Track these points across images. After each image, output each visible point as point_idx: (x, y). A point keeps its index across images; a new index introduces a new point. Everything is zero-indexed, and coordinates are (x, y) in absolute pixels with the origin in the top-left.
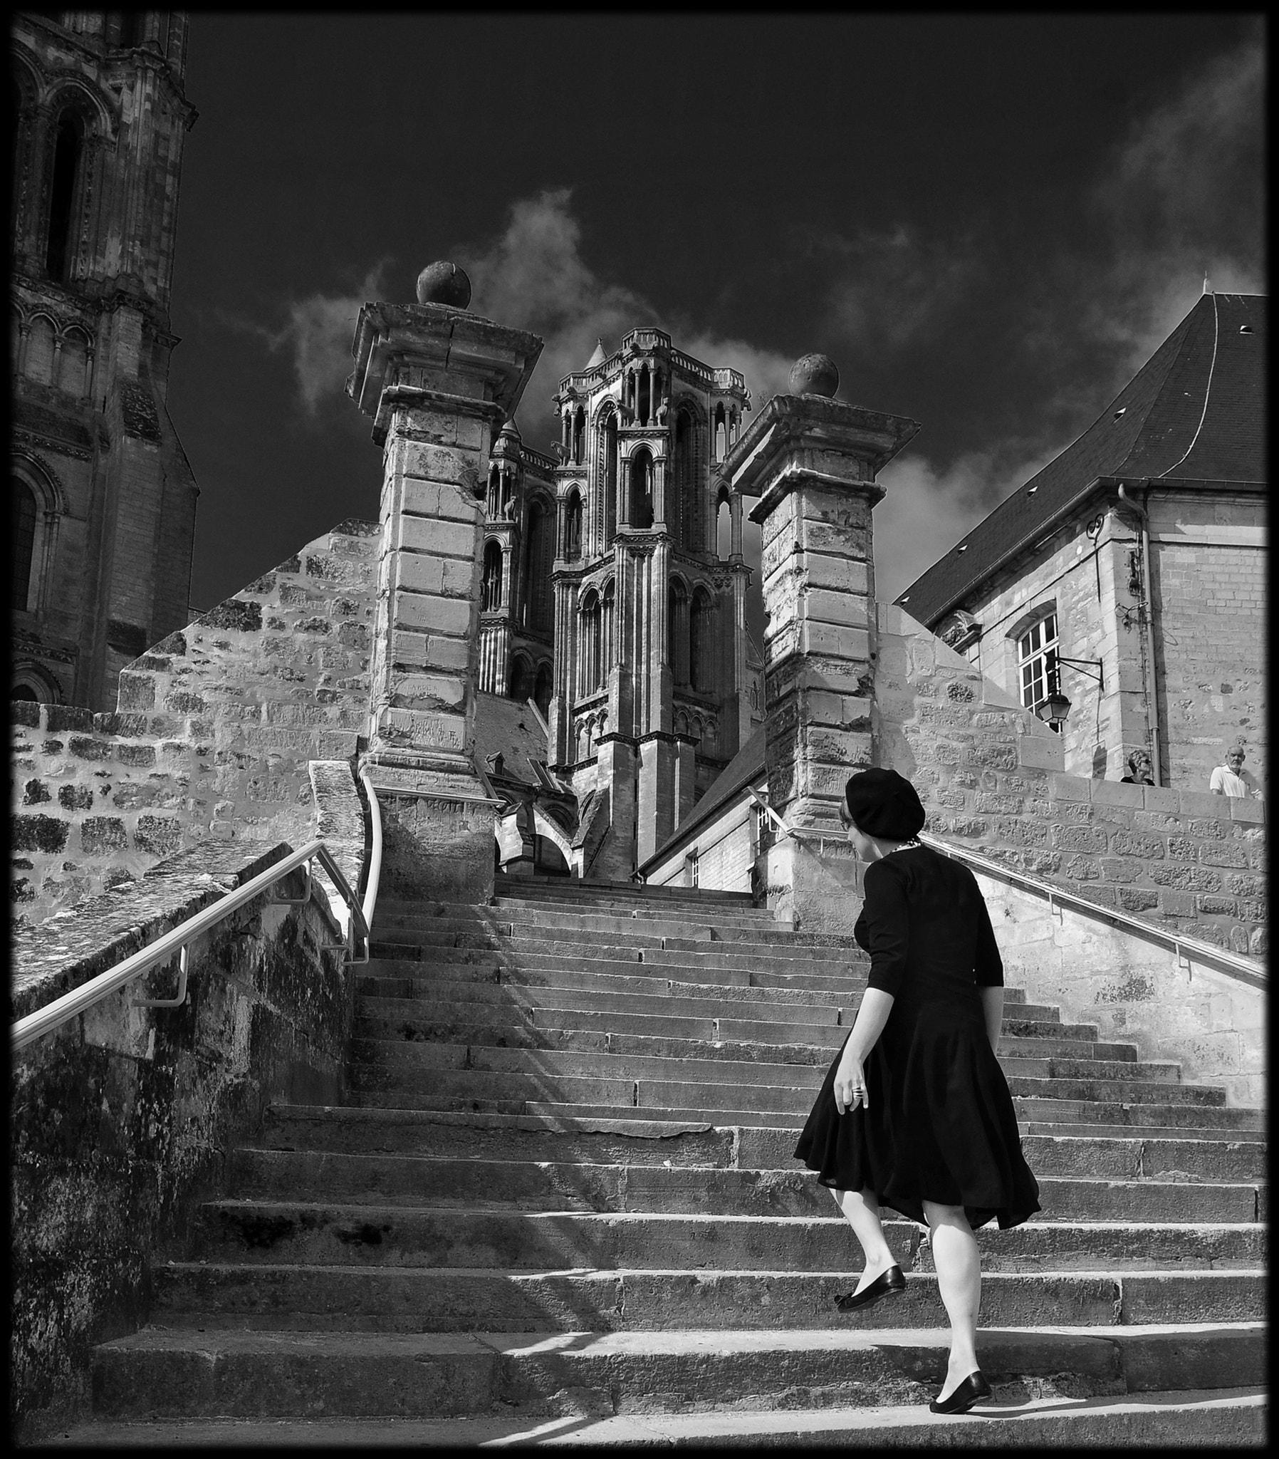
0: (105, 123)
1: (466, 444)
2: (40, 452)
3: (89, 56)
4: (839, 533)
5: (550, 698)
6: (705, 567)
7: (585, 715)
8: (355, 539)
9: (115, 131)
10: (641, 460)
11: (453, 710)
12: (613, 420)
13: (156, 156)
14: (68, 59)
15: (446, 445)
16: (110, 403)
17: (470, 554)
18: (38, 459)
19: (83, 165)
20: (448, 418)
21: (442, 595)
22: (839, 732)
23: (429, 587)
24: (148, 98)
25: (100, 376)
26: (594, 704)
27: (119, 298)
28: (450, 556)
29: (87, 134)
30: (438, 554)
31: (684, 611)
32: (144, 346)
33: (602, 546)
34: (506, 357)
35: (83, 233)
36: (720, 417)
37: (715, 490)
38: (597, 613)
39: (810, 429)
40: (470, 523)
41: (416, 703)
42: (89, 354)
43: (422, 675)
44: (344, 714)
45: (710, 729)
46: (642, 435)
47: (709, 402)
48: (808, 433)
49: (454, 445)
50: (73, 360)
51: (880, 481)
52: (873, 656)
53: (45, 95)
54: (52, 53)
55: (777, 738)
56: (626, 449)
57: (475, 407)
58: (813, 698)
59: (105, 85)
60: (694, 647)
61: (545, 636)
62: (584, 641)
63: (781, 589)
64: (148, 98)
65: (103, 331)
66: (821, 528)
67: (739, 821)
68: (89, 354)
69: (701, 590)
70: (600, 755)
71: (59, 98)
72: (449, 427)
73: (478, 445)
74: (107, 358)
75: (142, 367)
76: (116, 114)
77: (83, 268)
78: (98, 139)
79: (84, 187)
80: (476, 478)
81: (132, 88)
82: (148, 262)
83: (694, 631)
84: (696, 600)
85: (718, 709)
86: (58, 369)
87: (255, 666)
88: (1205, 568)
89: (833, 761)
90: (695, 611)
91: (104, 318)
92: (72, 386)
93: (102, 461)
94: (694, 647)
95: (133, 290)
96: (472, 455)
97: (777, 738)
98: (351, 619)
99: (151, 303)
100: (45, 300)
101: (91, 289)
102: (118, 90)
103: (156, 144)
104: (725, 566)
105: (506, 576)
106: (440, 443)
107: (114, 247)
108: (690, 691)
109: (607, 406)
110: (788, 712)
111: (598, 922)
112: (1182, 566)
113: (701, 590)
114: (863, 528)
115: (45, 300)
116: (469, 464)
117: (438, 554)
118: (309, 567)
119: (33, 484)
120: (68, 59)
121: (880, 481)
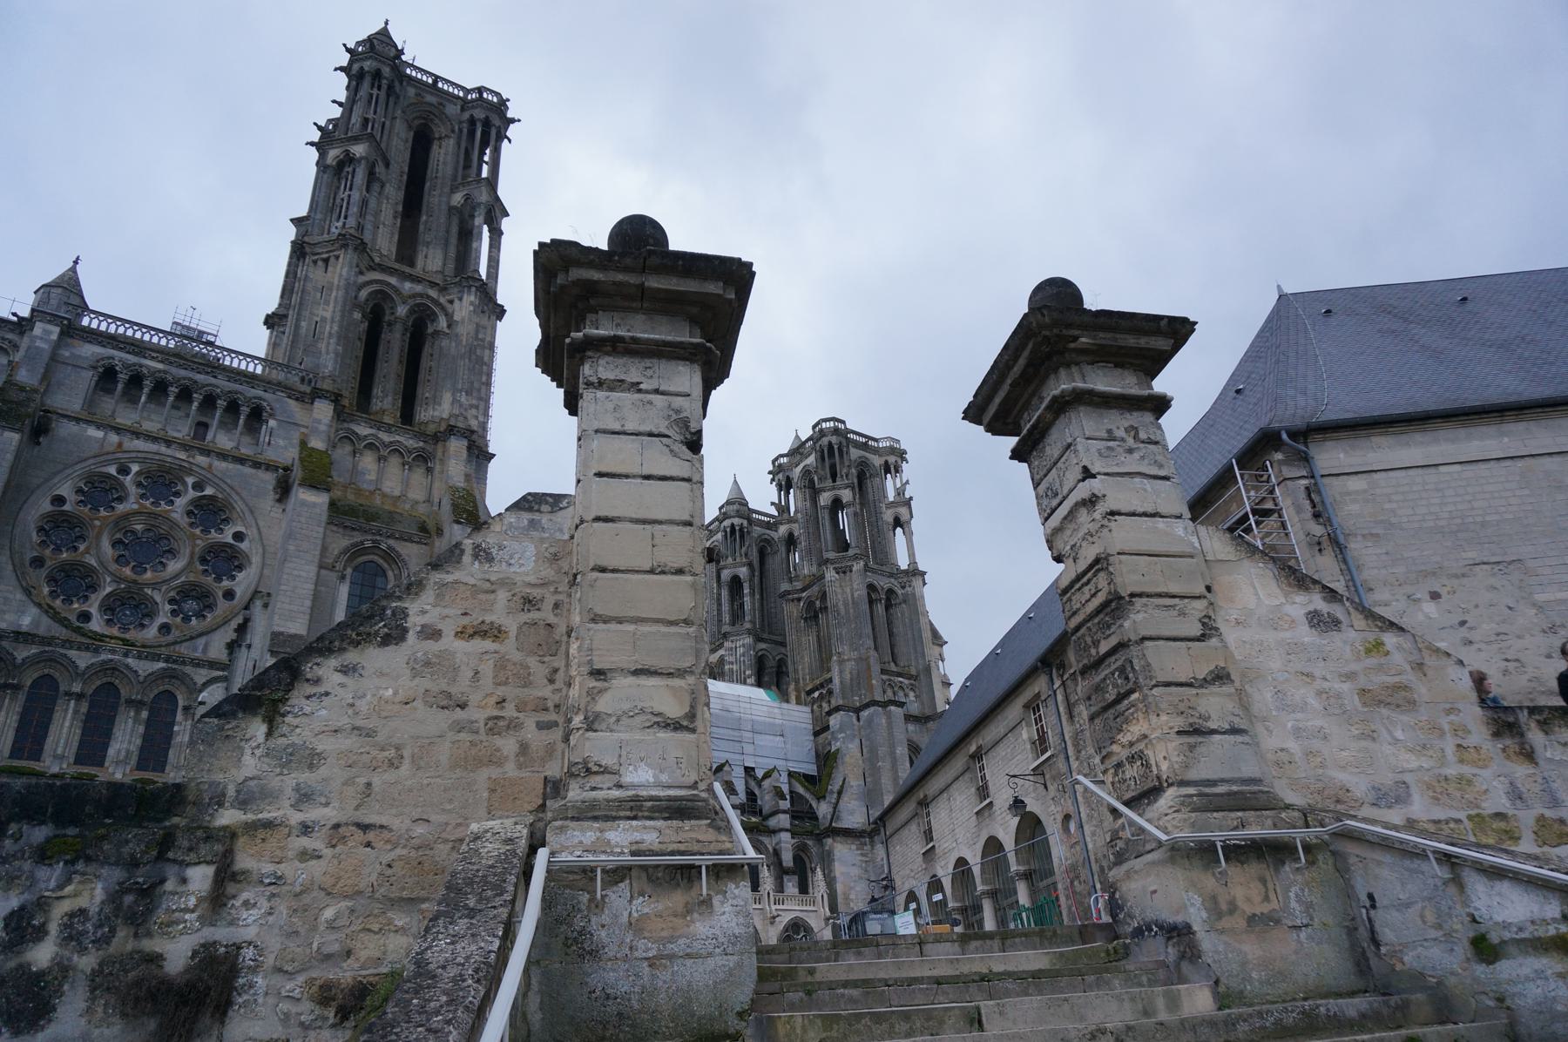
0: (442, 323)
1: (672, 389)
2: (391, 542)
3: (433, 284)
4: (1130, 451)
5: (788, 684)
6: (891, 575)
7: (816, 694)
8: (536, 516)
9: (449, 326)
10: (837, 504)
11: (676, 726)
12: (812, 481)
13: (477, 338)
14: (419, 288)
15: (647, 392)
16: (444, 502)
17: (686, 517)
18: (389, 547)
19: (427, 350)
20: (648, 362)
21: (652, 572)
22: (1194, 691)
23: (635, 564)
24: (472, 303)
25: (436, 485)
26: (822, 685)
27: (451, 430)
28: (660, 522)
29: (430, 330)
30: (644, 522)
31: (880, 609)
32: (469, 461)
33: (814, 569)
34: (713, 288)
35: (424, 392)
36: (888, 471)
37: (891, 520)
38: (816, 617)
39: (1075, 339)
40: (683, 480)
41: (625, 720)
42: (429, 470)
43: (631, 680)
44: (524, 748)
45: (912, 694)
46: (834, 488)
47: (877, 461)
48: (1072, 345)
49: (657, 391)
50: (418, 476)
51: (1160, 385)
52: (1209, 589)
53: (402, 310)
54: (408, 285)
55: (1106, 709)
56: (825, 499)
57: (680, 345)
58: (1134, 651)
59: (442, 300)
60: (891, 634)
61: (779, 639)
62: (809, 640)
63: (1072, 526)
64: (472, 303)
65: (439, 454)
66: (1109, 448)
67: (961, 770)
68: (429, 470)
69: (890, 592)
70: (831, 723)
71: (412, 311)
72: (649, 373)
73: (686, 389)
74: (442, 472)
75: (467, 477)
76: (449, 316)
77: (423, 414)
78: (437, 333)
79: (425, 363)
80: (687, 427)
81: (460, 299)
82: (472, 406)
83: (889, 623)
84: (888, 599)
85: (916, 678)
86: (406, 484)
87: (395, 694)
88: (1378, 491)
89: (1196, 731)
90: (888, 607)
91: (440, 445)
92: (417, 494)
93: (437, 544)
94: (891, 634)
95: (460, 425)
96: (678, 402)
97: (1106, 709)
98: (534, 615)
99: (473, 432)
100: (398, 438)
101: (431, 428)
102: (451, 302)
103: (477, 332)
104: (906, 572)
105: (747, 599)
106: (640, 391)
107: (447, 398)
108: (893, 667)
109: (806, 472)
110: (1122, 670)
111: (899, 966)
112: (1357, 492)
113: (890, 592)
114: (1156, 443)
115: (398, 438)
116: (678, 412)
117: (644, 522)
118: (476, 556)
119: (385, 565)
120: (419, 288)
121: (1160, 385)
